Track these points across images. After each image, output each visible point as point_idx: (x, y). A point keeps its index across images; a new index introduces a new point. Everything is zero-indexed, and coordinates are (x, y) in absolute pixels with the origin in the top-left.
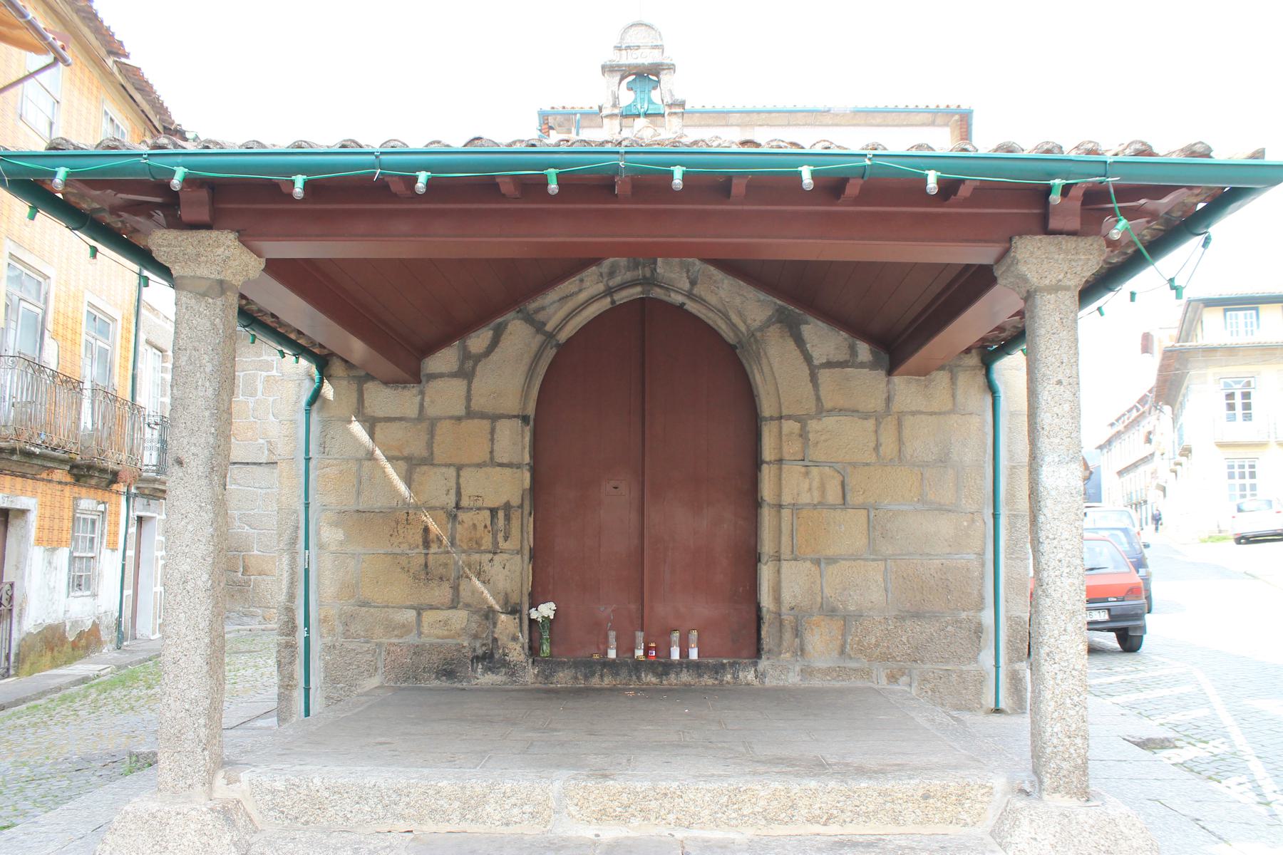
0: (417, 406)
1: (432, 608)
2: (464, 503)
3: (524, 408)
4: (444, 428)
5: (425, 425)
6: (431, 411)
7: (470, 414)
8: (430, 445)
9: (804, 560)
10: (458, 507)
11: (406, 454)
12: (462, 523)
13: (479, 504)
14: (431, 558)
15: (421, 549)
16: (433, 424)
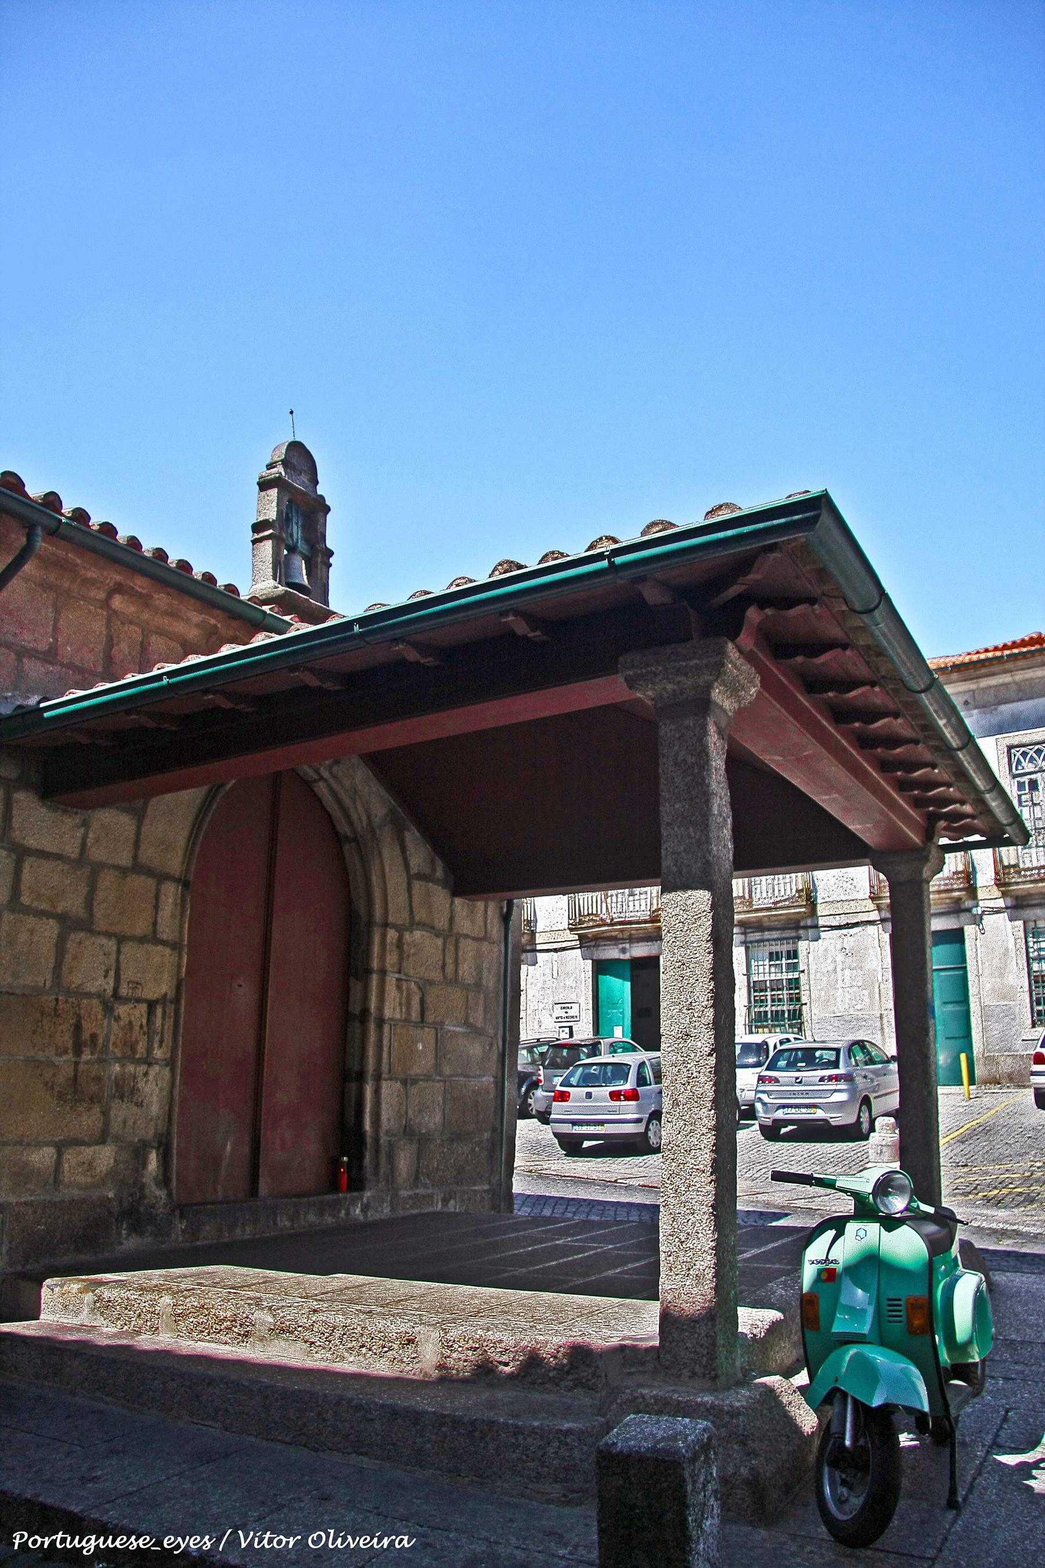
0: (79, 841)
1: (77, 1142)
2: (124, 991)
3: (187, 871)
4: (107, 880)
5: (87, 871)
6: (97, 854)
7: (138, 868)
8: (89, 902)
9: (397, 1079)
10: (116, 994)
11: (59, 910)
12: (118, 1019)
13: (138, 993)
14: (81, 1067)
15: (70, 1056)
16: (97, 870)
